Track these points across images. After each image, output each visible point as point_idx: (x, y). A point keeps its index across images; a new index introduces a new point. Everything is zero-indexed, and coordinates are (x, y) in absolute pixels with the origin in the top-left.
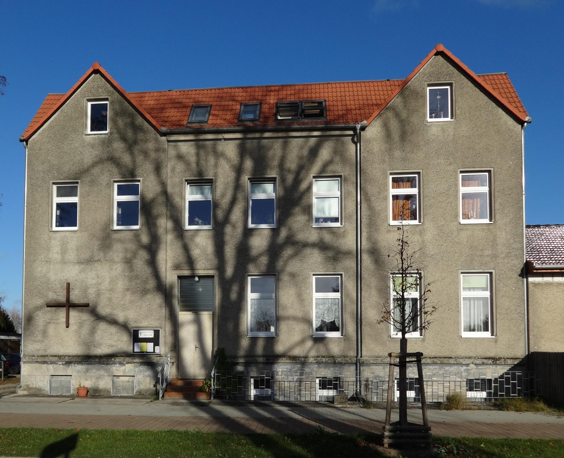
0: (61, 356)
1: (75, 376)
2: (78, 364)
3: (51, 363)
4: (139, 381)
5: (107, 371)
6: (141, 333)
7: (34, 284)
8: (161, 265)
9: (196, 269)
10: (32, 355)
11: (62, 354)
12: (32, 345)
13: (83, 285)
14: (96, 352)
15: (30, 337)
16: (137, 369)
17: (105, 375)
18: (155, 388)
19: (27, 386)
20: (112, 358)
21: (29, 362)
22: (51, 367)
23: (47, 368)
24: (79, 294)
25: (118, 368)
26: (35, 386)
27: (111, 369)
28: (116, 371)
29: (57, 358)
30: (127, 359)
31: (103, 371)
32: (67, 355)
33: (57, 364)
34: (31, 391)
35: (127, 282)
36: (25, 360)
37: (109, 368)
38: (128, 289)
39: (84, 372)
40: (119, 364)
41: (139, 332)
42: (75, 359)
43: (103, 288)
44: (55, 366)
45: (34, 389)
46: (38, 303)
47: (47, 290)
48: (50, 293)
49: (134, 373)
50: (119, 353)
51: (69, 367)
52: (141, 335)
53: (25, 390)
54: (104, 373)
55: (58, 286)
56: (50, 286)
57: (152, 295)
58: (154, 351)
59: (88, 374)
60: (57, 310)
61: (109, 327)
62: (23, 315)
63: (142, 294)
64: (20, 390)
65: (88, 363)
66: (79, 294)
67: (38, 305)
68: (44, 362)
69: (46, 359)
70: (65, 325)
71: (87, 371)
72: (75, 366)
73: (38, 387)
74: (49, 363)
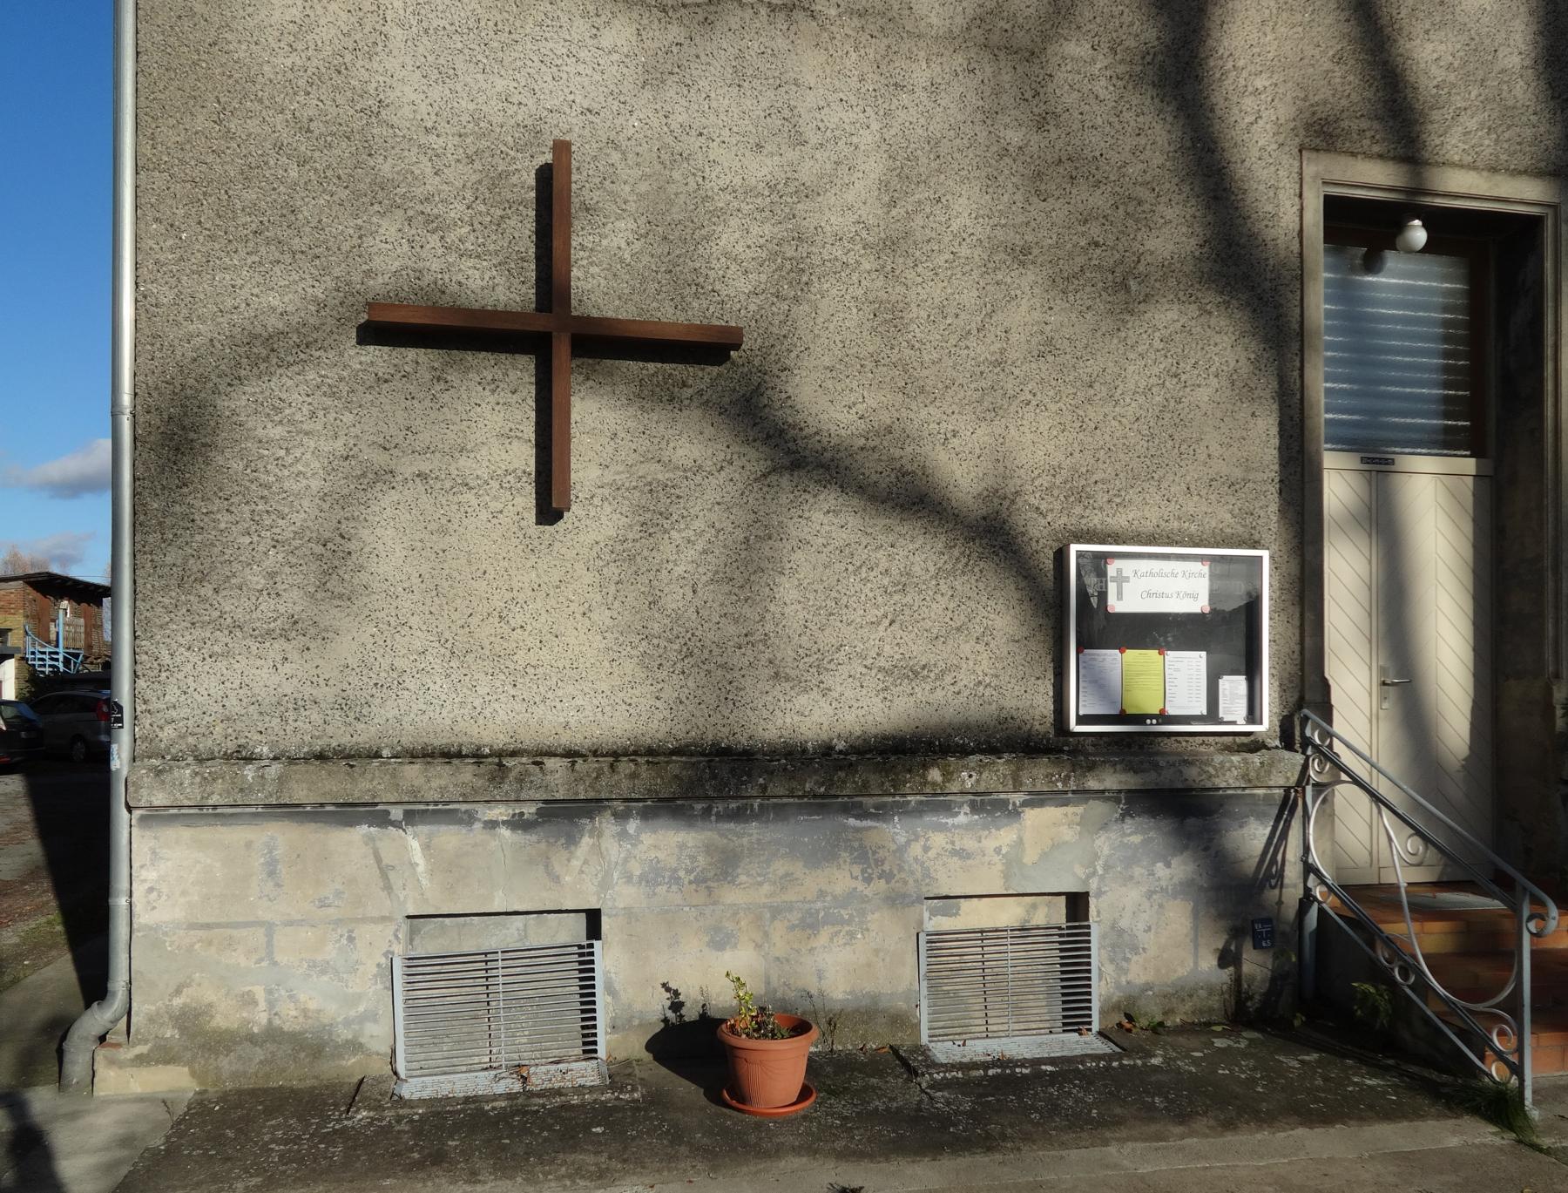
0: (500, 754)
1: (630, 914)
2: (647, 815)
3: (411, 817)
4: (1121, 932)
5: (866, 857)
6: (1121, 579)
7: (229, 135)
8: (1249, 103)
9: (1437, 164)
10: (231, 746)
11: (501, 740)
12: (222, 665)
13: (672, 189)
14: (790, 719)
15: (207, 590)
16: (1105, 843)
17: (864, 899)
18: (1226, 975)
19: (191, 1022)
20: (925, 767)
21: (203, 814)
22: (415, 844)
23: (378, 860)
24: (646, 259)
25: (969, 843)
26: (263, 1018)
27: (916, 849)
28: (955, 862)
29: (467, 773)
30: (1039, 773)
31: (857, 870)
32: (548, 741)
33: (469, 819)
34: (226, 1064)
35: (1019, 197)
36: (159, 799)
37: (902, 840)
38: (1026, 251)
39: (699, 881)
40: (974, 808)
41: (1112, 568)
42: (633, 776)
43: (836, 221)
44: (449, 837)
45: (252, 1039)
46: (274, 300)
47: (358, 195)
48: (389, 228)
49: (1080, 872)
50: (965, 728)
51: (572, 841)
52: (1120, 596)
53: (163, 1055)
54: (860, 886)
55: (460, 174)
56: (386, 169)
57: (1193, 310)
58: (1212, 715)
59: (732, 896)
60: (453, 376)
61: (889, 529)
62: (126, 399)
63: (1122, 296)
64: (112, 1062)
65: (733, 805)
66: (646, 259)
67: (274, 323)
68: (348, 812)
69: (367, 784)
70: (526, 500)
71: (726, 865)
72: (623, 835)
73: (289, 1018)
74: (397, 813)
